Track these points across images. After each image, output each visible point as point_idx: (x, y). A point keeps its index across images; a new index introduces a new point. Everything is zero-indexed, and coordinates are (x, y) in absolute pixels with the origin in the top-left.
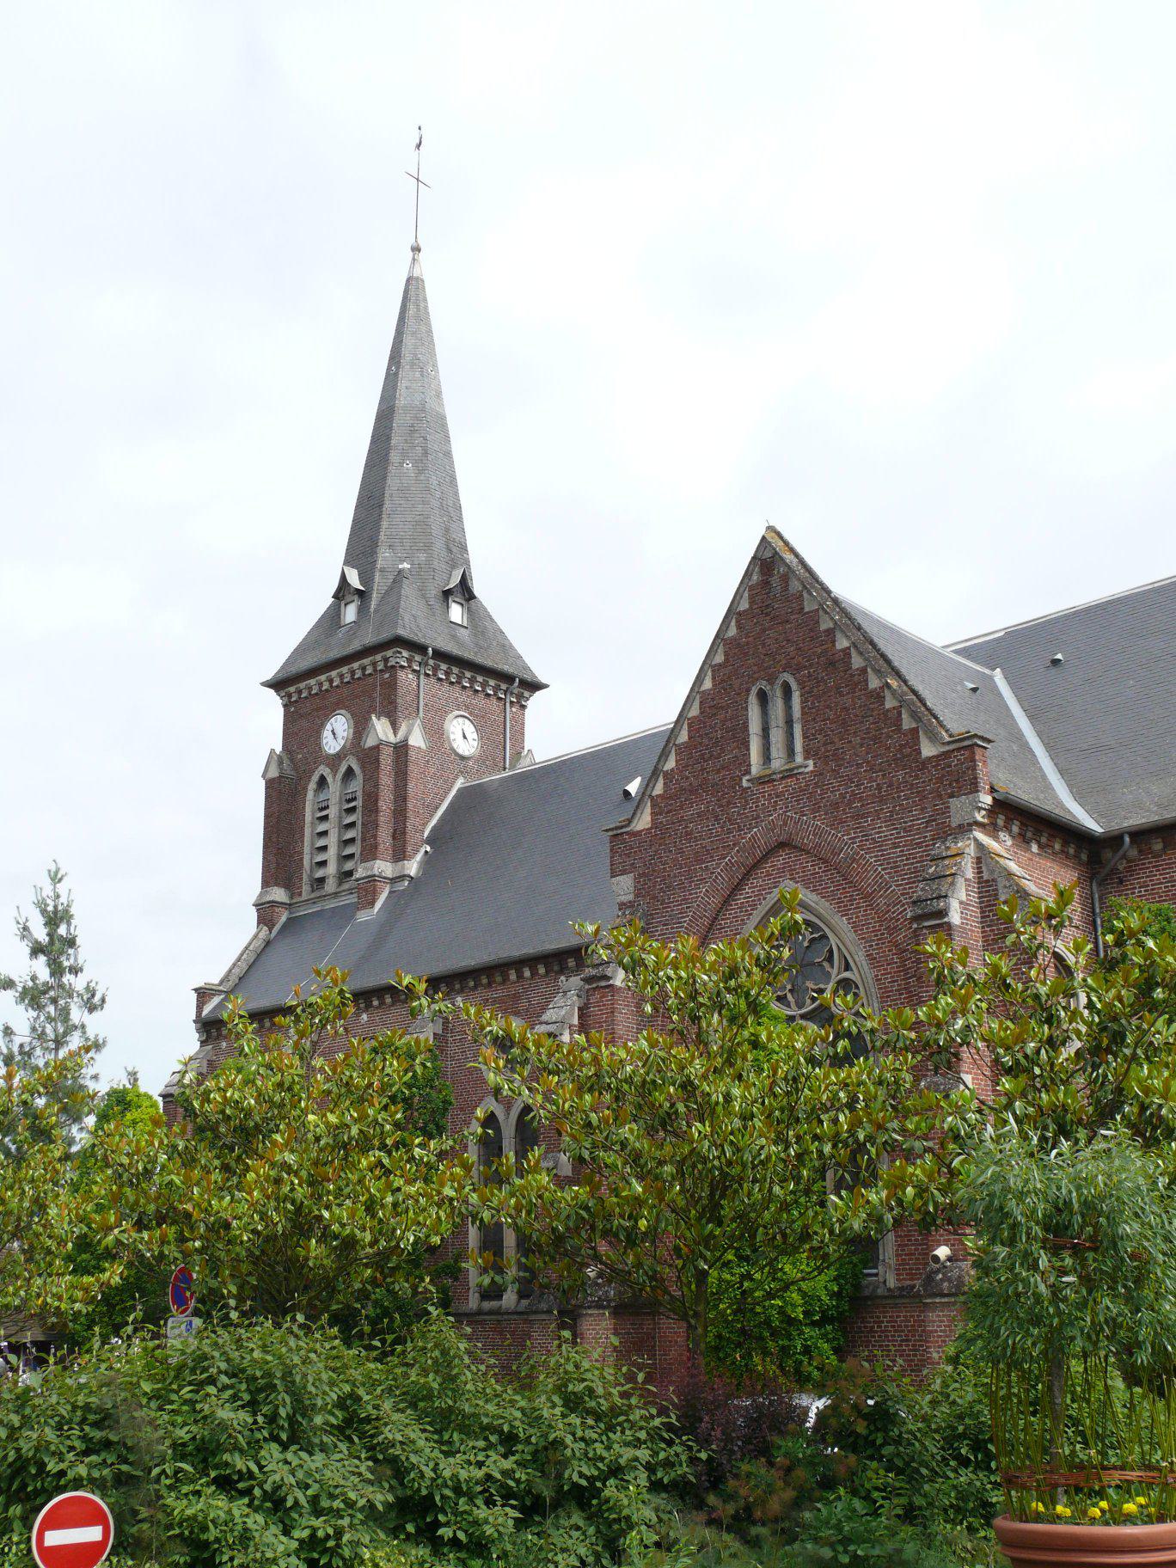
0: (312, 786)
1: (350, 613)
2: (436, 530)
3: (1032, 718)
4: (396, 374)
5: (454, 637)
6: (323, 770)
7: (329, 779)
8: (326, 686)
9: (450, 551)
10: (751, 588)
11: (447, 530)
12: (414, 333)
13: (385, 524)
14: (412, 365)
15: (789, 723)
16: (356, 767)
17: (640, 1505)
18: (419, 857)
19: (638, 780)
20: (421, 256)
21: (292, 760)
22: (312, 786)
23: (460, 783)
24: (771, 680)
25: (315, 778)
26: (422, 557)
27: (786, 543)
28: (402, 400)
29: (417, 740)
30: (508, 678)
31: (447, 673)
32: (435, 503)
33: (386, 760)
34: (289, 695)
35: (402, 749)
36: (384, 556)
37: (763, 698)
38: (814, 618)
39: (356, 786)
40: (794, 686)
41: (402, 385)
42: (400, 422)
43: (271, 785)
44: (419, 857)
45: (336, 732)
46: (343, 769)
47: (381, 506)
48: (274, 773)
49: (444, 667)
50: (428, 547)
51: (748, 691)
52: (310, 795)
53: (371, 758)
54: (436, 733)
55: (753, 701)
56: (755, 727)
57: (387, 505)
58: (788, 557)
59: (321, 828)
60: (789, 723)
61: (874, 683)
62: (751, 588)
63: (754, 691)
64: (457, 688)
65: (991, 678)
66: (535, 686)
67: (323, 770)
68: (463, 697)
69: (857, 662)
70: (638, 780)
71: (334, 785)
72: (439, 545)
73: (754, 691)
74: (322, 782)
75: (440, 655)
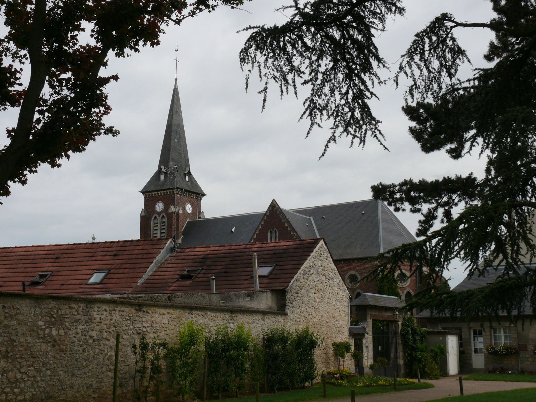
0: (153, 218)
1: (162, 177)
2: (183, 158)
3: (318, 230)
4: (172, 115)
5: (187, 185)
6: (156, 215)
7: (158, 218)
8: (156, 195)
9: (186, 162)
10: (270, 211)
11: (185, 157)
12: (176, 104)
13: (171, 156)
14: (176, 113)
15: (276, 237)
16: (165, 215)
17: (323, 318)
18: (181, 238)
19: (234, 228)
20: (177, 81)
21: (147, 211)
22: (153, 218)
23: (188, 220)
24: (273, 229)
25: (154, 216)
26: (180, 164)
27: (277, 203)
28: (174, 122)
29: (181, 212)
30: (198, 194)
31: (186, 194)
32: (182, 150)
33: (175, 217)
34: (146, 195)
35: (178, 213)
36: (171, 164)
37: (271, 232)
38: (281, 219)
39: (165, 220)
40: (277, 231)
41: (174, 118)
42: (174, 128)
43: (142, 217)
44: (181, 238)
45: (159, 207)
46: (161, 216)
47: (170, 150)
48: (143, 214)
49: (185, 193)
50: (181, 162)
51: (268, 230)
52: (152, 220)
53: (170, 216)
54: (184, 209)
55: (269, 232)
56: (269, 237)
57: (171, 151)
58: (277, 206)
59: (155, 228)
60: (276, 237)
61: (292, 233)
62: (270, 211)
63: (269, 231)
64: (188, 197)
65: (310, 219)
66: (203, 195)
67: (156, 215)
68: (188, 198)
69: (289, 229)
70: (234, 228)
71: (159, 220)
72: (183, 161)
73: (269, 231)
74: (156, 218)
75: (185, 190)
